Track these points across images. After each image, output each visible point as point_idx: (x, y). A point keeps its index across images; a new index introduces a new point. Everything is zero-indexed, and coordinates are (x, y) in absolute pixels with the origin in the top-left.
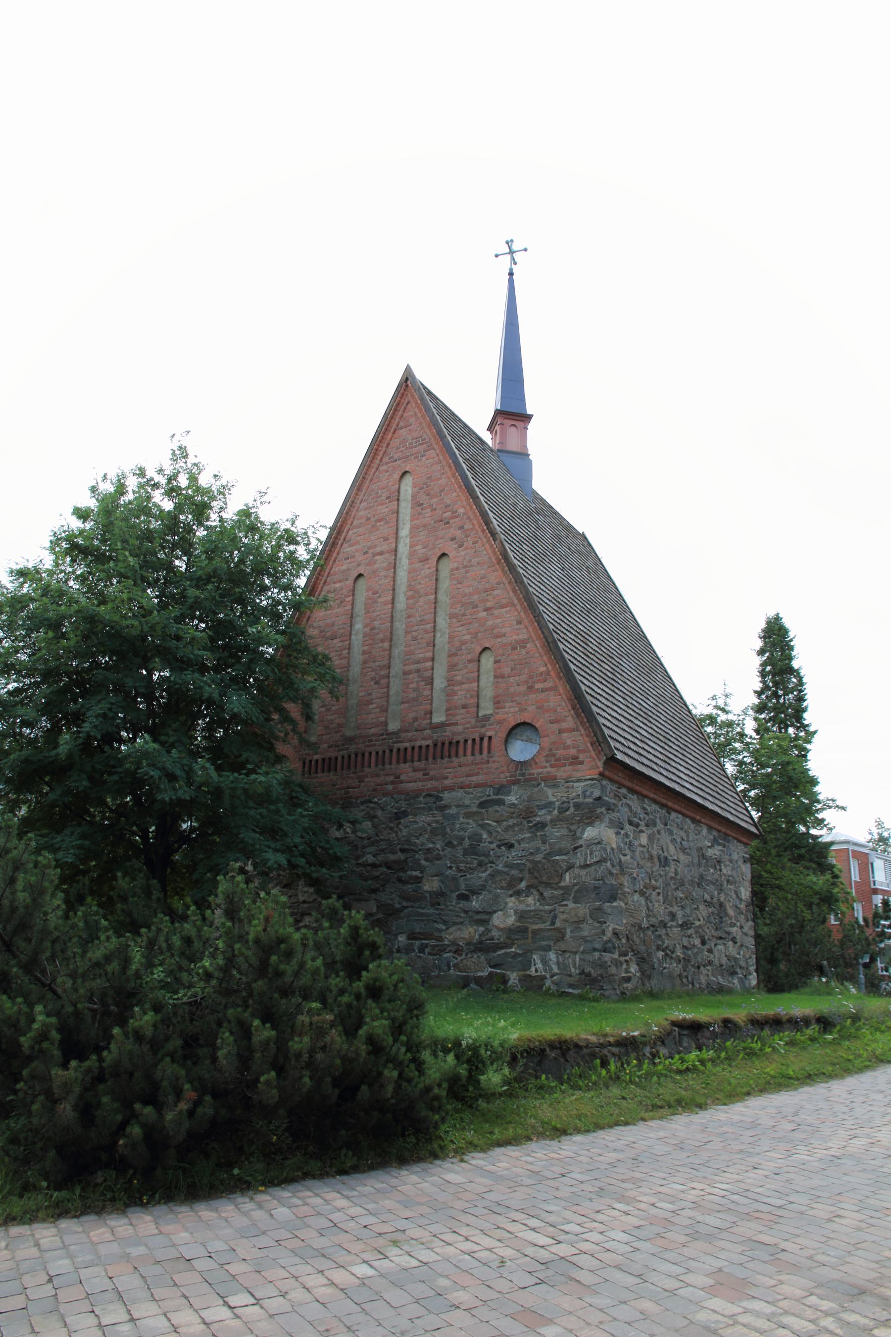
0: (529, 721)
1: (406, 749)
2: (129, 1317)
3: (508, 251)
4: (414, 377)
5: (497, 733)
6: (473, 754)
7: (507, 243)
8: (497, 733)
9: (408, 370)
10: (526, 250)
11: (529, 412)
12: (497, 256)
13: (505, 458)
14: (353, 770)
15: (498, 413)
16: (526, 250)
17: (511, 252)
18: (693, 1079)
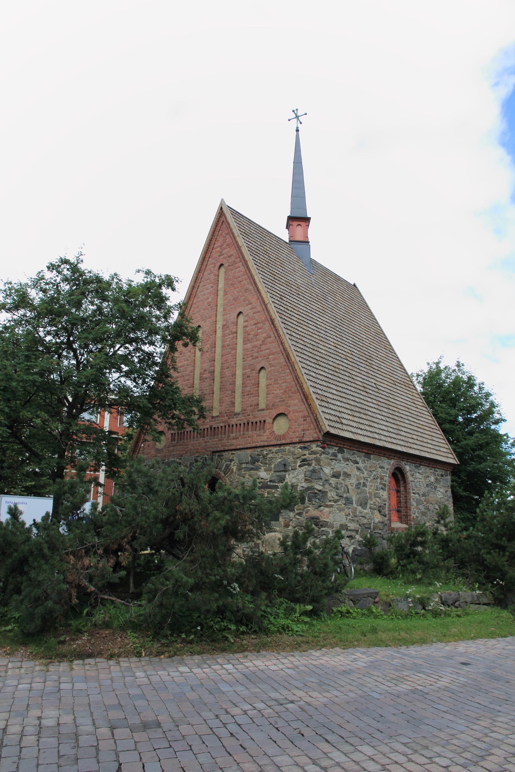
0: (283, 412)
1: (222, 427)
2: (115, 731)
3: (295, 116)
4: (224, 202)
5: (268, 417)
6: (187, 439)
7: (294, 111)
8: (268, 417)
9: (222, 199)
10: (306, 114)
11: (308, 216)
12: (289, 120)
13: (295, 246)
14: (196, 439)
15: (291, 219)
16: (306, 114)
17: (297, 117)
18: (86, 679)
